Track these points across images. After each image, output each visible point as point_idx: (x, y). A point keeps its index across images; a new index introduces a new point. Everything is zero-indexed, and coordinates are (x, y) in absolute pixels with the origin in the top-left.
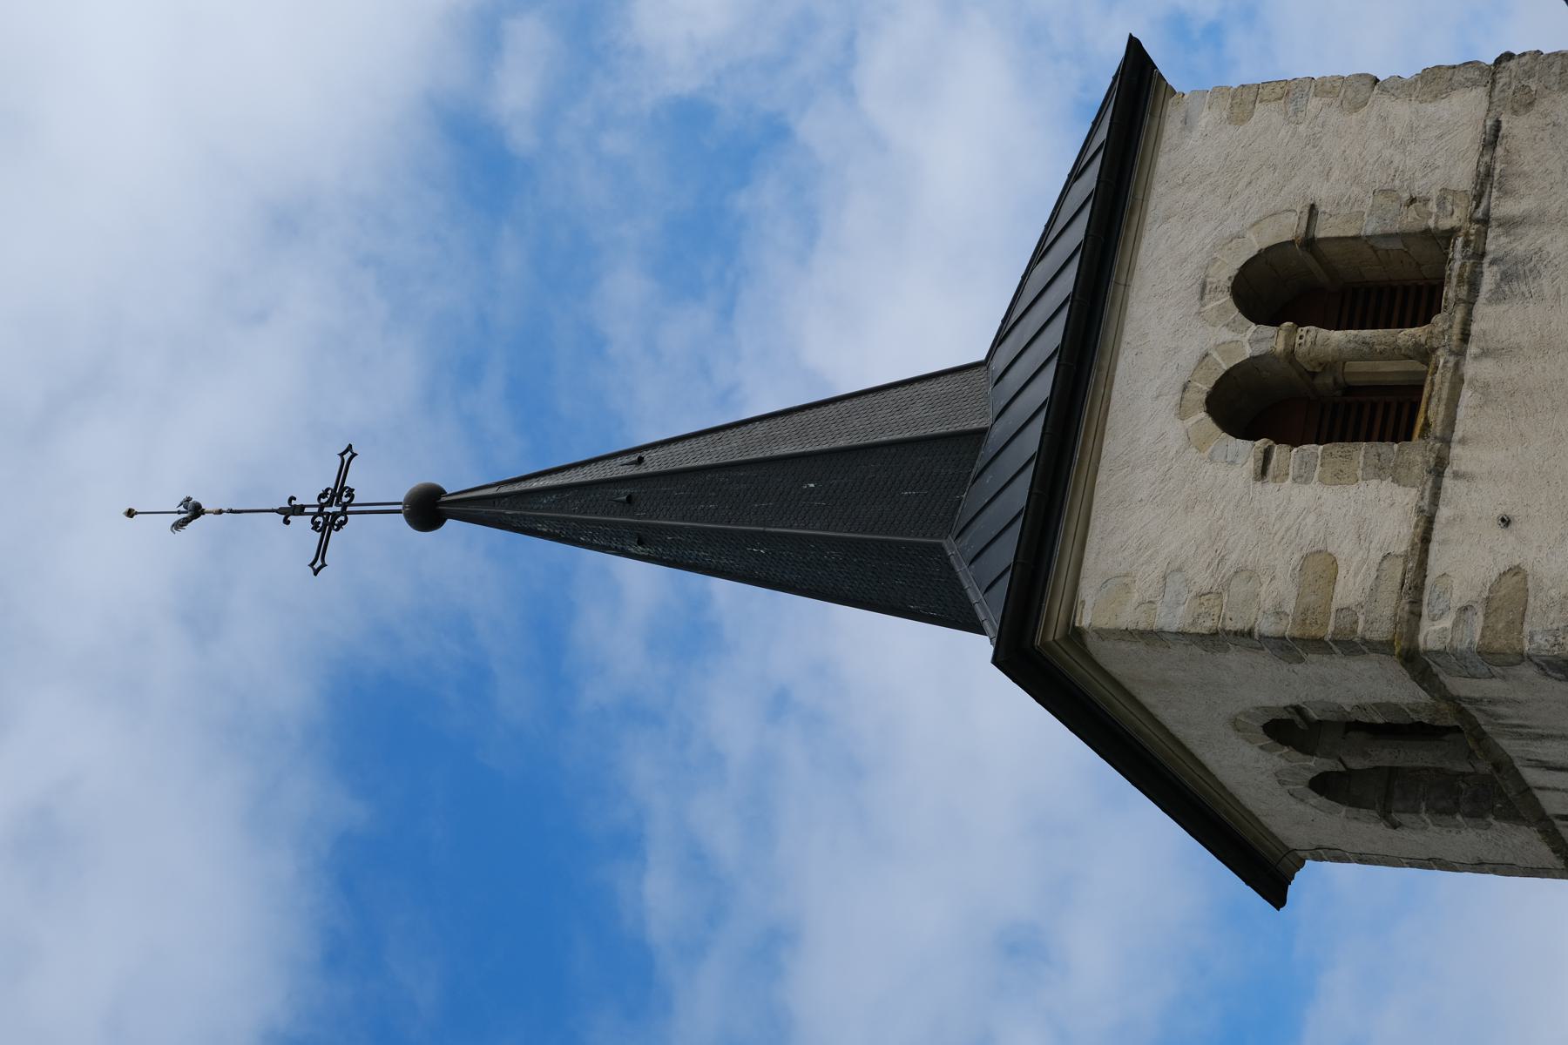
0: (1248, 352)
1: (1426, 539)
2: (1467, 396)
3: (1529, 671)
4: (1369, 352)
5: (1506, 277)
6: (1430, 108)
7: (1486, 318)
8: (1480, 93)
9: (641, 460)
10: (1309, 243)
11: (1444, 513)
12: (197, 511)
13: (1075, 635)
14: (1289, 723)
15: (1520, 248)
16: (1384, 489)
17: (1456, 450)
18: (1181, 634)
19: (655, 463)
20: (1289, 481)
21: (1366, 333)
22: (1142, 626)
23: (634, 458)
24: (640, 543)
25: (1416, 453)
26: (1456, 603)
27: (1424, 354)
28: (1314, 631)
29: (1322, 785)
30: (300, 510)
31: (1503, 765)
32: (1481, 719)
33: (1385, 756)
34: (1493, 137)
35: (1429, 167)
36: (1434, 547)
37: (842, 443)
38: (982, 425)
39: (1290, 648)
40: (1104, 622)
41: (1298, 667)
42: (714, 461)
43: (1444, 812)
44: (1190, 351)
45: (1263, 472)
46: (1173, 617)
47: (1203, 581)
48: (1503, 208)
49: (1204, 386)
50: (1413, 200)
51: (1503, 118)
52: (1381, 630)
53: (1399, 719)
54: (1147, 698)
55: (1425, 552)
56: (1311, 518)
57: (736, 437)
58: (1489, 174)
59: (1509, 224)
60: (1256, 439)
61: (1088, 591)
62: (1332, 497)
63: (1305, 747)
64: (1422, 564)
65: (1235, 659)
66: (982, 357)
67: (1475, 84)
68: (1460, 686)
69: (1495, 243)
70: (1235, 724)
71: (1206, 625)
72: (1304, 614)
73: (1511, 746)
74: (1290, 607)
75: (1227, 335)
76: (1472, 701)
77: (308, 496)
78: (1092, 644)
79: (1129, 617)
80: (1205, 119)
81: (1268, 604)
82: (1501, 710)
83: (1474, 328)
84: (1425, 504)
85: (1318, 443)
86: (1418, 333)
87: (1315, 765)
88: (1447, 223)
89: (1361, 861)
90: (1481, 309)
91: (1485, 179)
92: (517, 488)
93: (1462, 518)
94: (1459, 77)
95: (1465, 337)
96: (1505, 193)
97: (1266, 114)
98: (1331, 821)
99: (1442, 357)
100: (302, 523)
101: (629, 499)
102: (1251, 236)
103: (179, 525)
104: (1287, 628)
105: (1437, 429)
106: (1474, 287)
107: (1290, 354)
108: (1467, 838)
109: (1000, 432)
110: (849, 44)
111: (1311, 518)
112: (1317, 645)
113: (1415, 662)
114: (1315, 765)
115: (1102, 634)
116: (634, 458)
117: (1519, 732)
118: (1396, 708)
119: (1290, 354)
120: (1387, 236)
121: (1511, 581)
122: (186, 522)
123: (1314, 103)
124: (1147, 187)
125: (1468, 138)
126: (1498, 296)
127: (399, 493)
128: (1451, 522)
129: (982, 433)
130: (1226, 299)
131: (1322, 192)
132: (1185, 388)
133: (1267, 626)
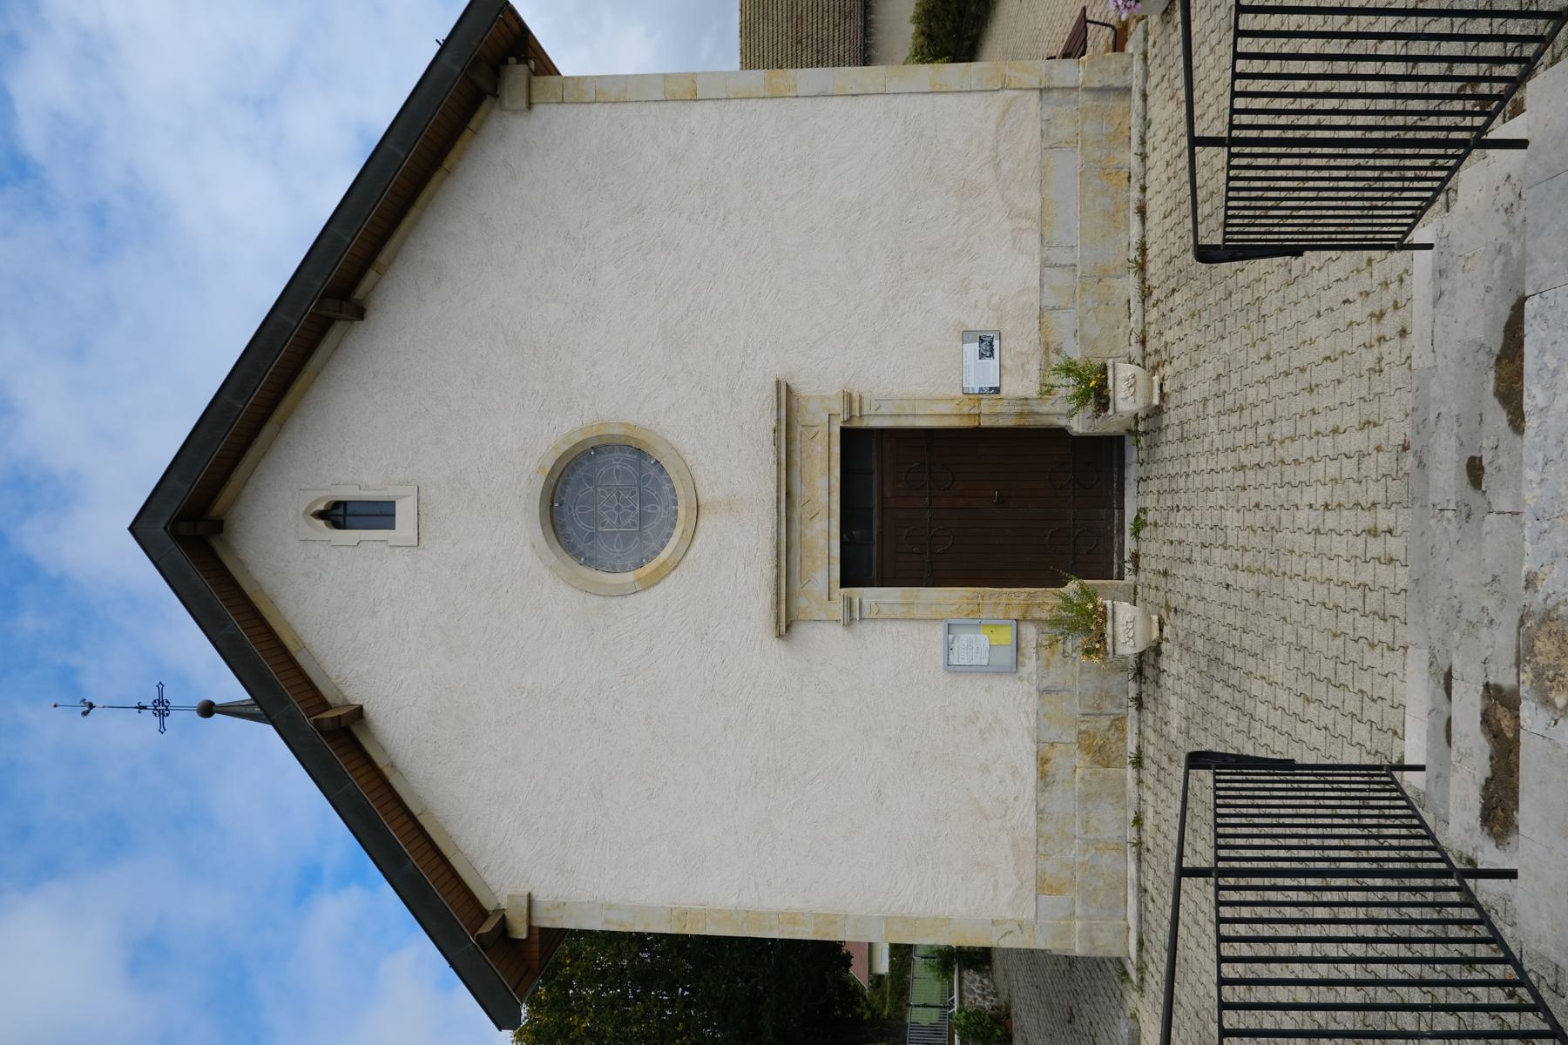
30: (145, 708)
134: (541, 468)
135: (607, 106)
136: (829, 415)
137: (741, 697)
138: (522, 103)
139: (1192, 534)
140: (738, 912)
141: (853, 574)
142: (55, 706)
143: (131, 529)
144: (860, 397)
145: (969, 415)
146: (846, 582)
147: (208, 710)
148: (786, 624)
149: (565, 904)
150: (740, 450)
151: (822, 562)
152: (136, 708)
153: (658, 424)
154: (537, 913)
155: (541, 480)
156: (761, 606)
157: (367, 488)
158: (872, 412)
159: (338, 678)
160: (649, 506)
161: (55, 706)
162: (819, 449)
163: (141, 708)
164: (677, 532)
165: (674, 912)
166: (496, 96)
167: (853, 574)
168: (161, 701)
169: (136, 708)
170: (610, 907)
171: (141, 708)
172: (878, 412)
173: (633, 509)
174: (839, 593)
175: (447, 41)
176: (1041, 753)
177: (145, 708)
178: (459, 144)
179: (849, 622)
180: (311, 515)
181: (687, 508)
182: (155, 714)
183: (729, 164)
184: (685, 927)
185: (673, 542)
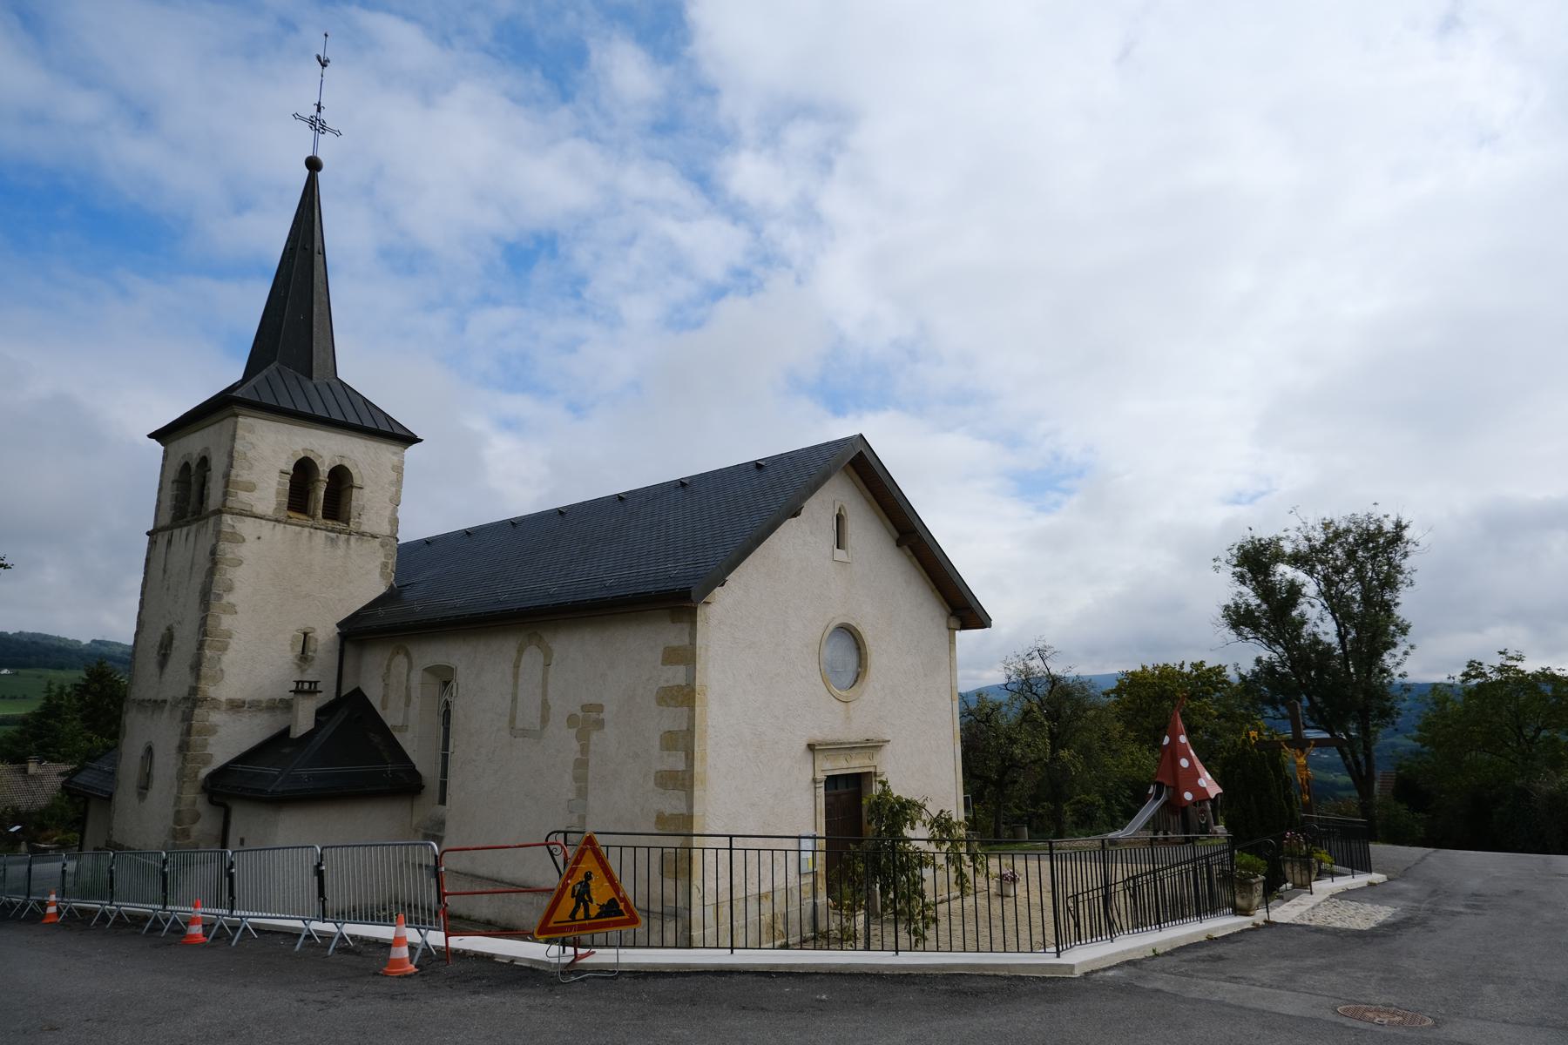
0: (321, 469)
1: (256, 517)
2: (298, 528)
3: (214, 541)
4: (317, 501)
5: (332, 539)
6: (387, 519)
7: (321, 534)
8: (388, 533)
9: (319, 253)
10: (352, 487)
11: (263, 522)
12: (324, 65)
13: (237, 416)
14: (206, 466)
15: (340, 543)
16: (273, 505)
17: (282, 525)
18: (233, 447)
19: (318, 258)
20: (278, 479)
21: (322, 501)
22: (237, 436)
23: (321, 251)
24: (291, 249)
25: (282, 515)
26: (235, 525)
27: (313, 517)
28: (231, 485)
29: (186, 466)
30: (319, 110)
31: (188, 523)
32: (202, 522)
33: (195, 488)
34: (374, 537)
35: (369, 520)
36: (253, 519)
37: (315, 329)
38: (314, 376)
39: (227, 476)
40: (239, 425)
41: (221, 476)
42: (315, 282)
43: (176, 498)
44: (322, 452)
45: (282, 472)
46: (239, 446)
47: (249, 454)
48: (353, 539)
49: (312, 456)
50: (360, 515)
51: (380, 540)
52: (229, 504)
53: (205, 498)
54: (217, 426)
55: (252, 517)
56: (266, 485)
57: (322, 290)
58: (363, 535)
59: (348, 541)
60: (293, 470)
61: (250, 420)
62: (273, 491)
63: (198, 465)
64: (248, 516)
65: (225, 459)
66: (339, 377)
67: (392, 532)
68: (212, 520)
69: (343, 537)
70: (207, 449)
71: (235, 455)
72: (236, 482)
73: (194, 527)
74: (239, 479)
75: (326, 464)
76: (207, 522)
77: (324, 115)
78: (234, 419)
79: (240, 432)
80: (395, 459)
81: (240, 473)
82: (204, 529)
83: (318, 531)
84: (267, 517)
85: (290, 489)
86: (320, 513)
87: (193, 466)
88: (351, 524)
89: (157, 505)
90: (324, 532)
91: (362, 534)
92: (316, 203)
93: (261, 526)
94: (395, 528)
95: (316, 528)
96: (357, 540)
97: (393, 475)
98: (176, 464)
99: (311, 522)
100: (314, 112)
101: (306, 249)
102: (356, 470)
103: (319, 58)
104: (233, 477)
105: (289, 521)
106: (332, 531)
107: (319, 481)
108: (168, 503)
109: (310, 385)
110: (598, 140)
111: (266, 485)
112: (227, 485)
113: (219, 512)
114: (193, 466)
115: (236, 423)
116: (321, 251)
117: (198, 531)
118: (208, 498)
119: (319, 481)
120: (350, 508)
121: (241, 540)
122: (320, 61)
123: (394, 489)
124: (377, 441)
125: (376, 530)
126: (327, 537)
127: (321, 156)
128: (261, 524)
129: (311, 378)
130: (338, 463)
131: (366, 491)
132: (312, 451)
133: (233, 472)
141: (832, 781)
142: (326, 35)
156: (818, 735)
170: (707, 650)
181: (847, 697)
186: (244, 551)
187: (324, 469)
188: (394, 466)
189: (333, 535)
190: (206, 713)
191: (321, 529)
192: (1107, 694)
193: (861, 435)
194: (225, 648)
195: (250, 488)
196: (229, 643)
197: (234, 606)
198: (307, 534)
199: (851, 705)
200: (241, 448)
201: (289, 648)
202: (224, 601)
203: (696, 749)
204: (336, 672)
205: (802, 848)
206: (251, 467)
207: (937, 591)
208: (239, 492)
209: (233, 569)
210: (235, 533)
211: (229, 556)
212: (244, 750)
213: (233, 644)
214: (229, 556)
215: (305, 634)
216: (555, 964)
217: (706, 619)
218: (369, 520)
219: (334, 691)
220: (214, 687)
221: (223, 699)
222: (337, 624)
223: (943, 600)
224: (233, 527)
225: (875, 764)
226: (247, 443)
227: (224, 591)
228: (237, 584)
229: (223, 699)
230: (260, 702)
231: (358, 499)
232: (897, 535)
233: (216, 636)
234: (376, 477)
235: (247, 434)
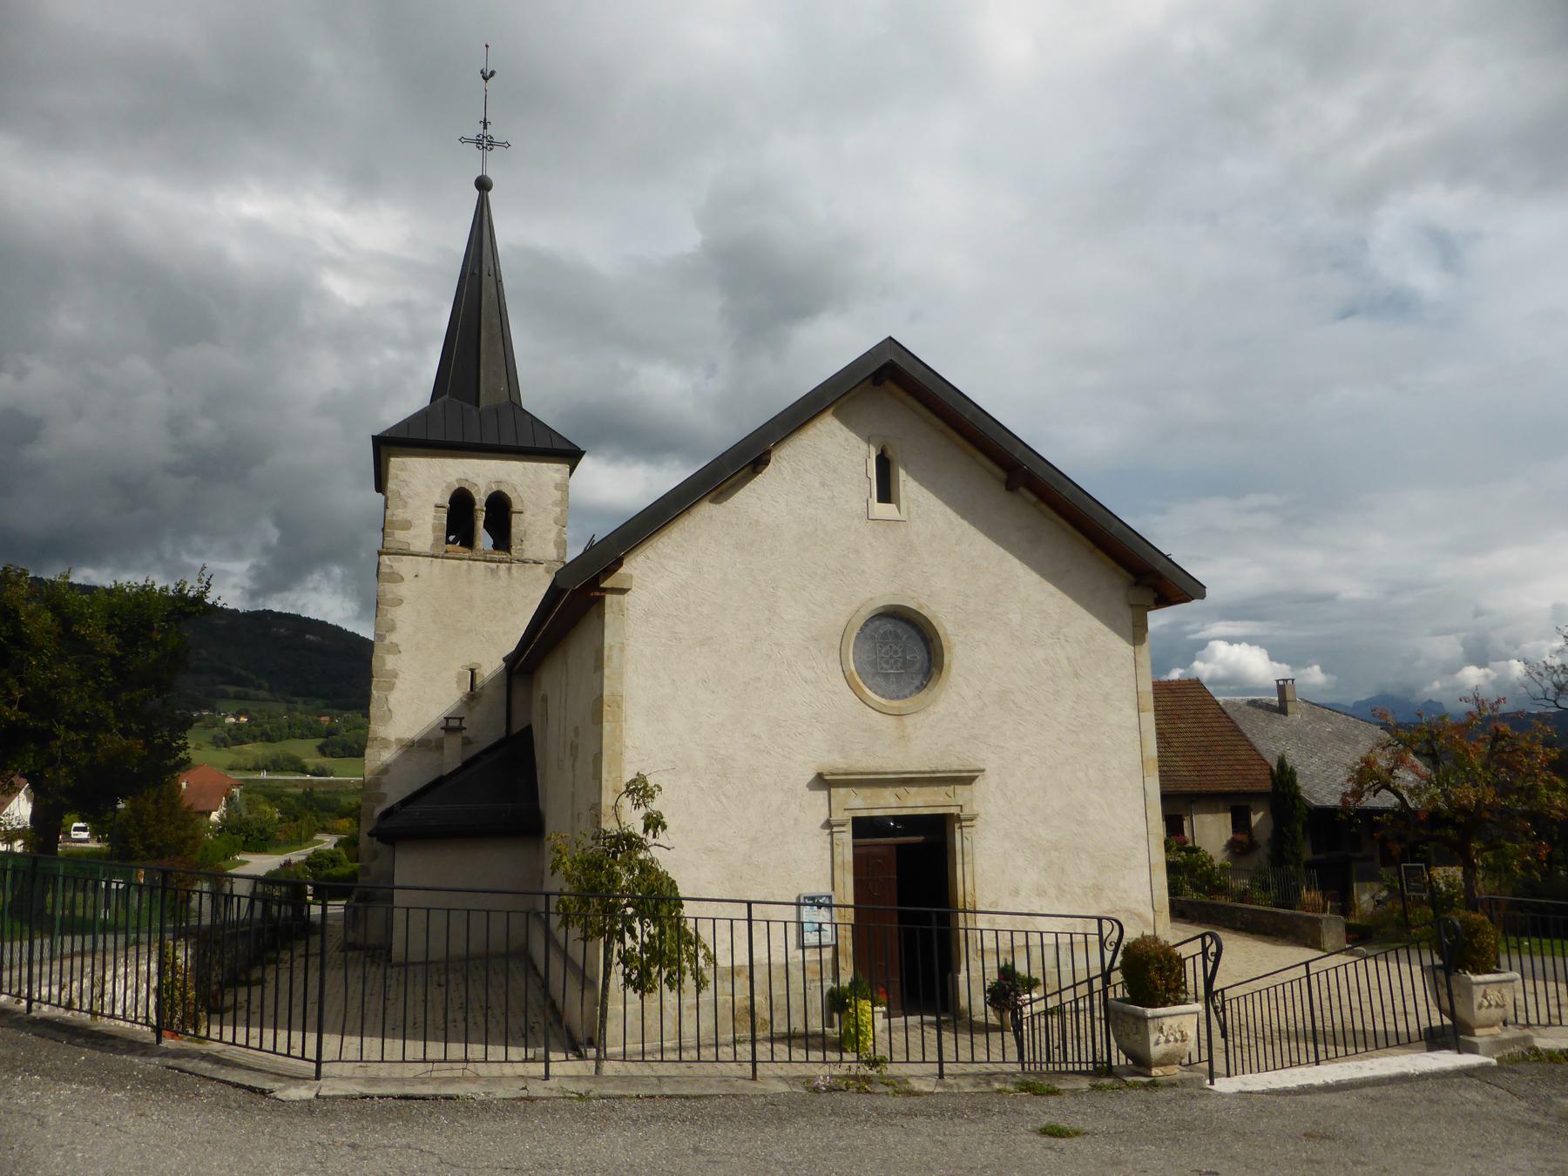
0: (477, 498)
11: (420, 559)
16: (430, 539)
17: (440, 560)
30: (485, 127)
47: (403, 493)
49: (505, 489)
59: (509, 569)
62: (429, 527)
64: (405, 555)
67: (558, 556)
69: (503, 566)
72: (392, 522)
74: (394, 518)
75: (482, 491)
77: (490, 131)
88: (513, 551)
97: (558, 495)
116: (492, 272)
125: (539, 556)
127: (490, 174)
130: (495, 489)
131: (527, 516)
132: (467, 480)
134: (921, 606)
135: (1133, 654)
136: (961, 806)
137: (776, 747)
138: (1133, 602)
139: (346, 1127)
140: (621, 746)
141: (864, 827)
142: (487, 46)
143: (890, 338)
144: (972, 826)
145: (965, 900)
146: (857, 822)
147: (483, 185)
148: (823, 782)
149: (623, 615)
150: (937, 744)
151: (869, 803)
152: (485, 119)
153: (951, 688)
154: (616, 597)
155: (913, 605)
156: (835, 761)
157: (905, 485)
158: (964, 835)
159: (779, 457)
160: (894, 679)
161: (487, 46)
162: (941, 799)
163: (485, 124)
164: (883, 701)
165: (619, 698)
166: (1136, 584)
167: (864, 827)
168: (491, 143)
169: (485, 119)
170: (622, 649)
171: (485, 124)
172: (964, 839)
173: (892, 668)
174: (848, 816)
175: (1170, 560)
176: (743, 968)
177: (485, 127)
178: (1109, 561)
179: (828, 825)
180: (884, 446)
181: (900, 708)
182: (479, 136)
183: (1104, 734)
184: (609, 706)
185: (877, 698)
186: (403, 590)
187: (480, 499)
188: (556, 484)
189: (493, 565)
190: (377, 753)
191: (479, 560)
192: (1468, 690)
193: (890, 338)
194: (391, 687)
195: (406, 525)
196: (395, 683)
197: (397, 646)
198: (466, 567)
199: (907, 720)
200: (394, 487)
201: (455, 686)
202: (387, 642)
203: (604, 775)
204: (504, 709)
205: (969, 927)
206: (405, 505)
207: (1097, 551)
208: (396, 531)
209: (393, 609)
210: (393, 573)
211: (388, 596)
212: (415, 790)
213: (399, 684)
214: (388, 596)
215: (472, 671)
216: (846, 1051)
217: (622, 610)
218: (532, 545)
219: (504, 728)
220: (383, 727)
221: (393, 738)
222: (504, 659)
223: (1114, 564)
224: (392, 567)
225: (960, 804)
226: (401, 481)
227: (387, 631)
228: (399, 624)
229: (393, 738)
230: (430, 741)
231: (518, 525)
232: (1003, 475)
233: (381, 677)
234: (537, 499)
235: (399, 473)
